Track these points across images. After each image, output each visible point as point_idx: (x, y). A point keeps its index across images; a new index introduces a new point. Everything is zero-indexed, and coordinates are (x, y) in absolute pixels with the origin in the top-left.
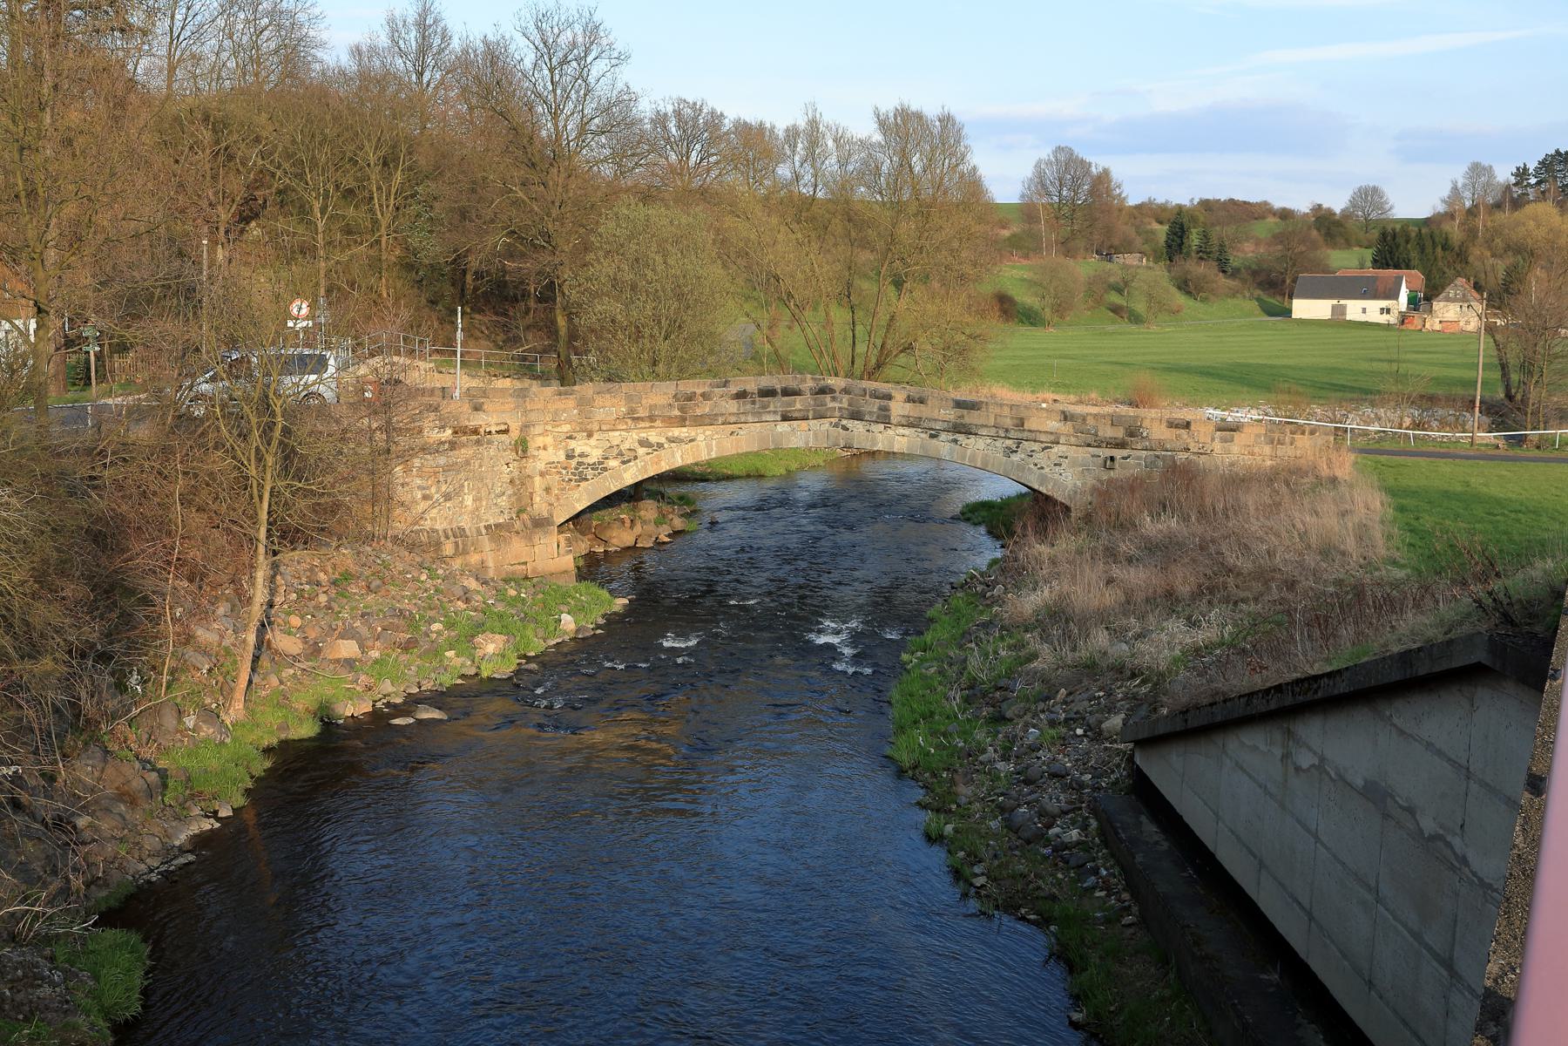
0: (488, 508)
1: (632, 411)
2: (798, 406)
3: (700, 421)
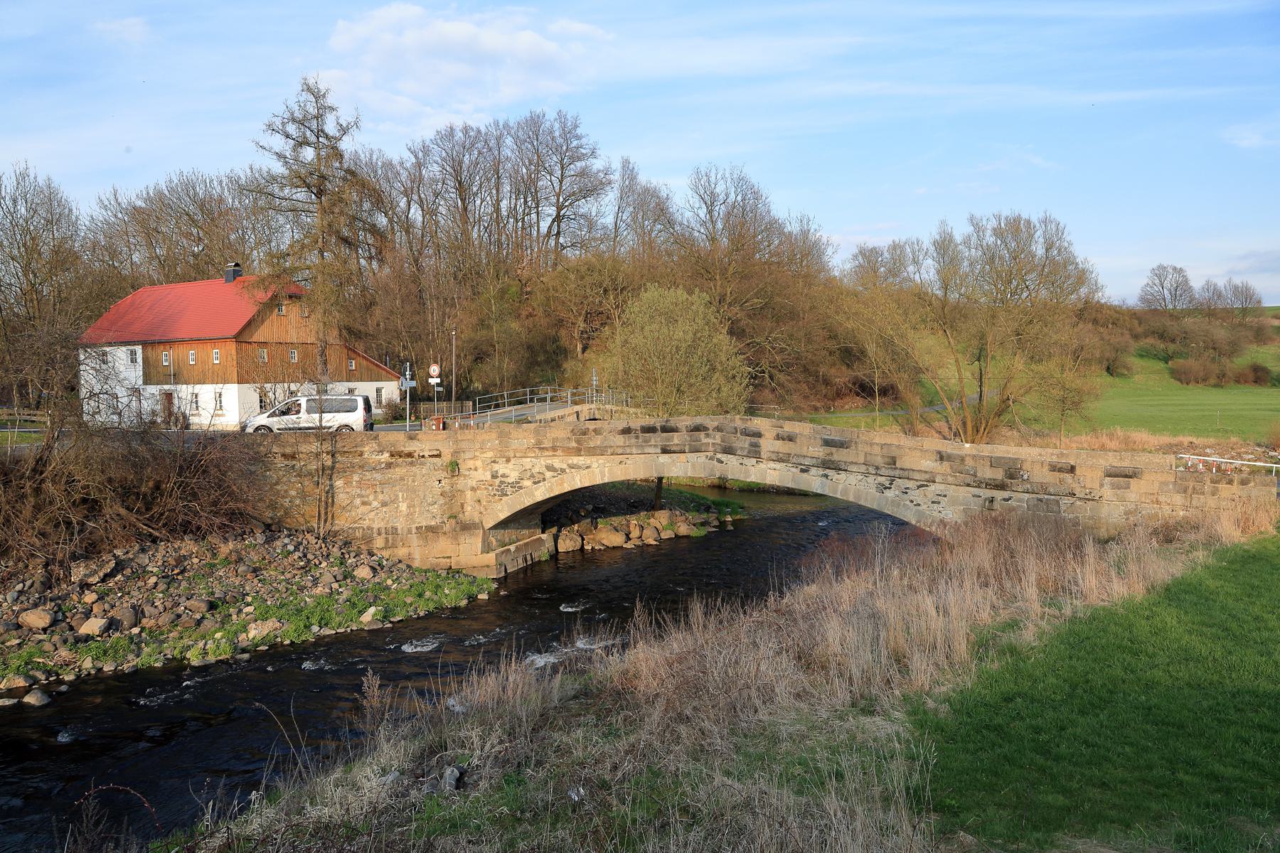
0: (421, 513)
1: (539, 442)
2: (676, 441)
3: (592, 452)
